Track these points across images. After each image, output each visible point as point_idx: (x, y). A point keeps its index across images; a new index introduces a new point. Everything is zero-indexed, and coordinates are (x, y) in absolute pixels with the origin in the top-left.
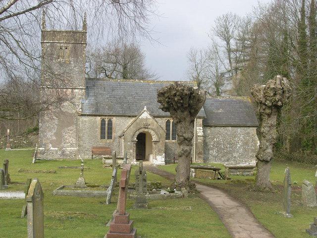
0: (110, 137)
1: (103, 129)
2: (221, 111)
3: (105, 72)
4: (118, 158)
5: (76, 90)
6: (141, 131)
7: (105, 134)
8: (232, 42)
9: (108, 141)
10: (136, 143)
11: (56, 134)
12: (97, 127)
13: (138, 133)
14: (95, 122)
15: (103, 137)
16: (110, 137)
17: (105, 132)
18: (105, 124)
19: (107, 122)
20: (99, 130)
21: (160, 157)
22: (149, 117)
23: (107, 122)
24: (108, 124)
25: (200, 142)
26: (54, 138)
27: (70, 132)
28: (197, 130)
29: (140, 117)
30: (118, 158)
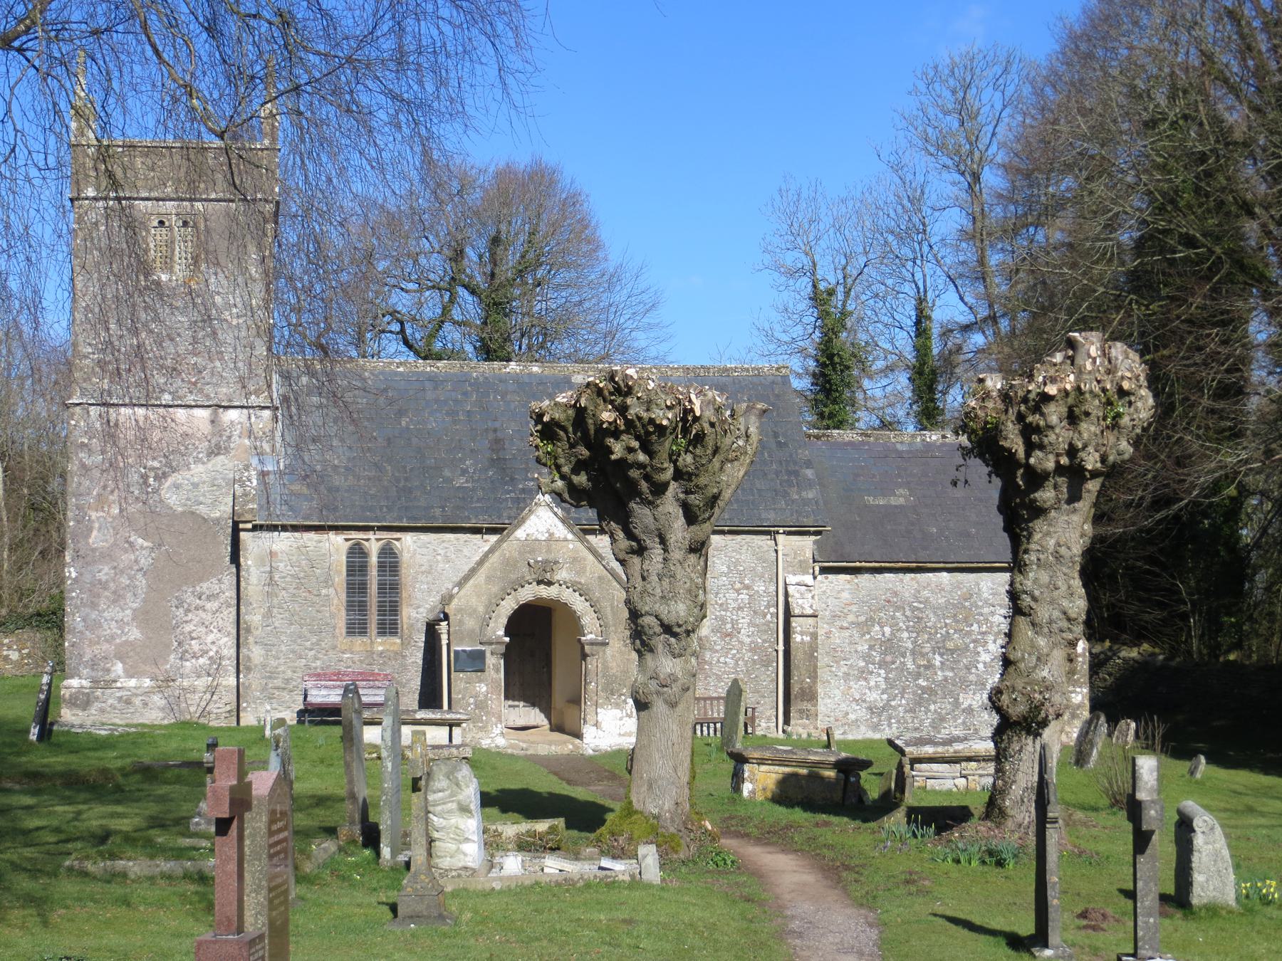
0: (389, 627)
1: (356, 587)
2: (901, 501)
3: (402, 331)
4: (986, 759)
5: (233, 415)
6: (528, 593)
7: (381, 606)
8: (992, 179)
9: (381, 644)
10: (502, 649)
11: (143, 617)
12: (327, 582)
13: (509, 606)
14: (964, 611)
15: (356, 628)
16: (389, 627)
17: (381, 611)
18: (363, 568)
19: (374, 559)
20: (337, 596)
21: (617, 713)
22: (561, 531)
23: (374, 559)
24: (381, 566)
25: (802, 642)
26: (135, 634)
27: (209, 606)
28: (791, 589)
29: (520, 533)
30: (986, 759)
